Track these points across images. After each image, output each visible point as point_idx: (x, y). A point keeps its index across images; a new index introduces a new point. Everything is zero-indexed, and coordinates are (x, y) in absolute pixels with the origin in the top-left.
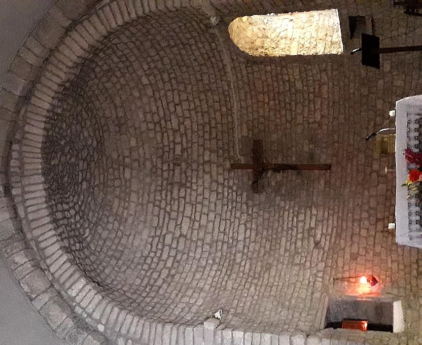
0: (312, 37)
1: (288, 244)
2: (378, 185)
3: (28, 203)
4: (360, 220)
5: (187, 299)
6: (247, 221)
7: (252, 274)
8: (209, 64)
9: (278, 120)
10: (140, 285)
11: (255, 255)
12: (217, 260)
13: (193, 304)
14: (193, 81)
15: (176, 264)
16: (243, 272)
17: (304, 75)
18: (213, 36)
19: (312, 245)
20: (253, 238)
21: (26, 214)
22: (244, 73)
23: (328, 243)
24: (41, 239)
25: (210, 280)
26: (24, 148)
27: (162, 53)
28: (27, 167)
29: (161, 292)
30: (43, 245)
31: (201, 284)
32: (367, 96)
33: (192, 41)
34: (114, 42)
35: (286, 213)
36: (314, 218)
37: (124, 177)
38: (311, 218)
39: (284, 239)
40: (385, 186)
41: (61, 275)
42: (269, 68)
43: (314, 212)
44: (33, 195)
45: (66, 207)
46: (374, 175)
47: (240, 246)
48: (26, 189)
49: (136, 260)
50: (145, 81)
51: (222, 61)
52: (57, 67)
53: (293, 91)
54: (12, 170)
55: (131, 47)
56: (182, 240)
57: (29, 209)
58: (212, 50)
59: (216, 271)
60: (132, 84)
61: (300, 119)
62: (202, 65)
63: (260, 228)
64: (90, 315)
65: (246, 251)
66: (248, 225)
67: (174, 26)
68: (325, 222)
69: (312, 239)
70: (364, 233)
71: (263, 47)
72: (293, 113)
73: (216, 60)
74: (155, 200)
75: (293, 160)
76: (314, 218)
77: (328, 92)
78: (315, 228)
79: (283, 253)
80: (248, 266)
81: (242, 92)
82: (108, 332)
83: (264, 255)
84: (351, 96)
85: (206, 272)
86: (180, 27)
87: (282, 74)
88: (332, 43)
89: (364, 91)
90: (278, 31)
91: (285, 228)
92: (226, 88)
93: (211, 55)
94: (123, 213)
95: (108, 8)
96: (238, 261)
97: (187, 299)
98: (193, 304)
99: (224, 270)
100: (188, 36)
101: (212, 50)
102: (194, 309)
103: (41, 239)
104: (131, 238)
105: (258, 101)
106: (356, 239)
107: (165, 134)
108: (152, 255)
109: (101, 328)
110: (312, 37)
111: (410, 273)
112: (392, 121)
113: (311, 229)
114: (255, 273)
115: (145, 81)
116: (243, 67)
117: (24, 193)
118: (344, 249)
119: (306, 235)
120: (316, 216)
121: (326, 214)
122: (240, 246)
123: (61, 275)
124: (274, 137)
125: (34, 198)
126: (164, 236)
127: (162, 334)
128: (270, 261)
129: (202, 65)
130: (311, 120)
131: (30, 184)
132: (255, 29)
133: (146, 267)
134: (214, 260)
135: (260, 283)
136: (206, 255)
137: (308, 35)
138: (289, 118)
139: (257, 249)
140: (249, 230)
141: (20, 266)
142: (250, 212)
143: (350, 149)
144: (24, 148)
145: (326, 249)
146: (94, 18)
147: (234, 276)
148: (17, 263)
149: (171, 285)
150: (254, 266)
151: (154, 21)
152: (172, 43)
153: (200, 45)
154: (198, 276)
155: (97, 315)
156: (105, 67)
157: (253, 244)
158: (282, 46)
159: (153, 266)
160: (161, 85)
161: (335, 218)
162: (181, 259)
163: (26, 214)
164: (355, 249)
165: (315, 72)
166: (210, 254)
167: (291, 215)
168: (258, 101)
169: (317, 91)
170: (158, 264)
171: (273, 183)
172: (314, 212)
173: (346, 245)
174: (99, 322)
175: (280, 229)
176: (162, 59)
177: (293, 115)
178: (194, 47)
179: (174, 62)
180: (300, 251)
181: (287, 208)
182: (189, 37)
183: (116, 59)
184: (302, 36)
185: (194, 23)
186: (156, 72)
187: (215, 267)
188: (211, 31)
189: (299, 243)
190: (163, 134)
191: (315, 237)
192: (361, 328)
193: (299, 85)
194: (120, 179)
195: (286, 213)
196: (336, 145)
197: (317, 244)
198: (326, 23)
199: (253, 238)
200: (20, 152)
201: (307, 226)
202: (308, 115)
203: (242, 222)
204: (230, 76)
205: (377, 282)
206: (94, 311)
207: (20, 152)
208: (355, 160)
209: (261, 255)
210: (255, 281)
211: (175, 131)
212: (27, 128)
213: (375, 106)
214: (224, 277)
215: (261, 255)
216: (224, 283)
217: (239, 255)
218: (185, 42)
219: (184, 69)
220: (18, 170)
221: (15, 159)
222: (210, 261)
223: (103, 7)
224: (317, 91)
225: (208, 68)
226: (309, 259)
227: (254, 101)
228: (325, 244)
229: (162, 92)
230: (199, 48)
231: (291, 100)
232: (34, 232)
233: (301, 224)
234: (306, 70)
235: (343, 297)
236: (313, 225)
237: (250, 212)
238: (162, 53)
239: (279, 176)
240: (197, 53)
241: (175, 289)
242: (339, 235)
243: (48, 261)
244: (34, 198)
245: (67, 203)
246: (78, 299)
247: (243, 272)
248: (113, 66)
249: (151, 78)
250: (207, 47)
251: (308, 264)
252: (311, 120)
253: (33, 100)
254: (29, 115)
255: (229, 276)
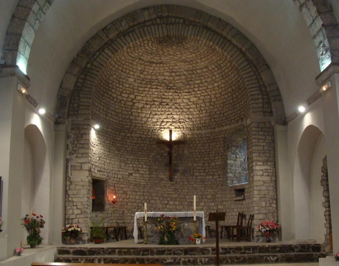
0: (236, 170)
1: (130, 160)
2: (161, 204)
3: (153, 27)
4: (143, 195)
5: (102, 108)
6: (142, 138)
7: (115, 141)
8: (224, 118)
9: (195, 154)
10: (109, 83)
11: (124, 143)
12: (121, 123)
13: (100, 112)
14: (215, 110)
15: (119, 101)
16: (116, 137)
17: (217, 167)
18: (238, 121)
19: (131, 172)
20: (133, 141)
21: (147, 26)
22: (220, 136)
23: (132, 180)
24: (134, 33)
25: (111, 119)
26: (181, 25)
27: (229, 94)
28: (171, 27)
29: (106, 95)
30: (131, 35)
31: (109, 115)
32: (206, 198)
33: (235, 110)
34: (235, 72)
35: (146, 159)
36: (144, 173)
37: (165, 72)
38: (143, 171)
39: (132, 157)
40: (161, 207)
41: (115, 45)
42: (221, 149)
43: (147, 173)
44: (156, 30)
45: (150, 44)
46: (166, 202)
47: (129, 135)
48: (160, 26)
49: (121, 80)
50: (216, 84)
51: (226, 125)
52: (222, 44)
53: (210, 161)
54: (170, 19)
55: (233, 79)
56: (131, 104)
57: (149, 28)
58: (231, 120)
59: (116, 123)
60: (214, 78)
61: (195, 165)
62: (224, 114)
63: (138, 145)
64: (95, 59)
65: (126, 138)
66: (139, 139)
67: (243, 102)
68: (142, 178)
69: (133, 172)
70: (137, 197)
71: (232, 146)
72: (198, 162)
73: (226, 122)
74: (152, 88)
75: (174, 162)
76: (144, 173)
77: (209, 179)
78: (139, 173)
79: (126, 157)
80: (119, 139)
81: (210, 135)
82: (87, 69)
83: (124, 147)
84: (207, 190)
85: (115, 117)
86: (242, 105)
87: (218, 155)
88: (233, 181)
89: (209, 197)
90: (240, 154)
91: (138, 158)
92: (212, 127)
93: (228, 120)
94: (146, 71)
95: (251, 70)
96: (121, 134)
97: (102, 108)
98: (100, 112)
99: (116, 127)
100: (238, 109)
101: (231, 120)
102: (97, 112)
103: (134, 33)
104: (133, 77)
105: (205, 143)
106: (134, 193)
107: (188, 94)
108: (124, 88)
109: (89, 66)
110: (236, 170)
111: (118, 219)
112: (269, 246)
113: (138, 171)
114: (115, 143)
115: (216, 84)
116: (223, 136)
117: (158, 25)
118: (129, 187)
119: (135, 169)
120: (145, 174)
121: (146, 179)
122: (129, 135)
123: (115, 45)
124: (186, 152)
125: (155, 30)
126: (134, 94)
127: (86, 98)
128: (122, 151)
129: (224, 114)
130: (195, 170)
131: (162, 28)
132: (241, 142)
133: (118, 85)
134: (122, 121)
135: (110, 145)
136: (124, 117)
137: (237, 168)
138: (196, 159)
139: (128, 144)
140: (137, 139)
141: (120, 23)
142: (147, 140)
143: (180, 190)
144: (181, 25)
145: (129, 179)
146: (246, 63)
147: (114, 132)
148: (121, 22)
149: (109, 99)
150: (119, 142)
151: (245, 92)
152: (234, 100)
153: (233, 114)
154: (113, 113)
155: (95, 63)
156: (222, 65)
157: (130, 141)
158: (232, 156)
159: (118, 89)
160: (213, 92)
161: (145, 183)
162: (121, 103)
163: (147, 26)
164: (129, 193)
165: (219, 172)
166: (124, 119)
167: (145, 161)
168: (205, 143)
169: (210, 173)
170: (119, 91)
171: (162, 151)
172: (147, 173)
173: (131, 188)
174: (92, 65)
175: (138, 155)
176: (227, 94)
177: (197, 162)
178: (232, 111)
179: (225, 100)
180: (127, 166)
181: (149, 159)
182: (238, 109)
183: (226, 71)
184: (237, 166)
185: (244, 113)
186: (220, 90)
187: (117, 122)
188: (240, 121)
189: (131, 165)
190: (188, 93)
191: (135, 173)
192: (193, 210)
193: (213, 164)
194: (164, 70)
195: (146, 159)
196: (182, 184)
197: (131, 174)
198: (242, 177)
199: (133, 141)
200: (179, 23)
201: (140, 169)
202: (197, 170)
203: (141, 136)
204: (217, 130)
205: (251, 216)
206: (97, 62)
207: (179, 23)
208: (174, 193)
209: (125, 146)
210: (111, 143)
211: (189, 99)
212: (191, 26)
213: (201, 202)
214: (113, 126)
215: (125, 146)
216: (110, 127)
217: (124, 134)
218: (236, 106)
219: (222, 105)
220: (169, 22)
221: (175, 21)
222: (120, 119)
223: (251, 67)
224: (210, 173)
225: (222, 117)
226: (123, 170)
227: (205, 141)
228: (131, 178)
229: (210, 93)
230: (232, 113)
231: (205, 161)
232: (138, 30)
233: (141, 166)
234: (220, 168)
235: (106, 187)
236: (141, 172)
237: (147, 140)
238: (229, 94)
239: (166, 155)
240: (230, 112)
241: (107, 101)
242: (135, 185)
243: (122, 38)
244: (155, 30)
245: (152, 45)
246: (103, 53)
247: (116, 137)
248: (223, 69)
249: (217, 88)
250: (233, 118)
251: (120, 170)
252: (195, 170)
253: (205, 31)
254: (198, 28)
255: (113, 129)
